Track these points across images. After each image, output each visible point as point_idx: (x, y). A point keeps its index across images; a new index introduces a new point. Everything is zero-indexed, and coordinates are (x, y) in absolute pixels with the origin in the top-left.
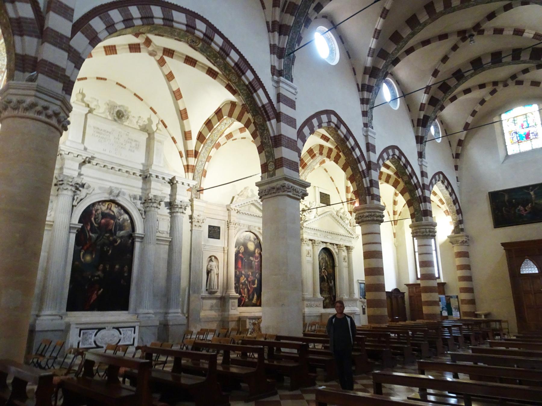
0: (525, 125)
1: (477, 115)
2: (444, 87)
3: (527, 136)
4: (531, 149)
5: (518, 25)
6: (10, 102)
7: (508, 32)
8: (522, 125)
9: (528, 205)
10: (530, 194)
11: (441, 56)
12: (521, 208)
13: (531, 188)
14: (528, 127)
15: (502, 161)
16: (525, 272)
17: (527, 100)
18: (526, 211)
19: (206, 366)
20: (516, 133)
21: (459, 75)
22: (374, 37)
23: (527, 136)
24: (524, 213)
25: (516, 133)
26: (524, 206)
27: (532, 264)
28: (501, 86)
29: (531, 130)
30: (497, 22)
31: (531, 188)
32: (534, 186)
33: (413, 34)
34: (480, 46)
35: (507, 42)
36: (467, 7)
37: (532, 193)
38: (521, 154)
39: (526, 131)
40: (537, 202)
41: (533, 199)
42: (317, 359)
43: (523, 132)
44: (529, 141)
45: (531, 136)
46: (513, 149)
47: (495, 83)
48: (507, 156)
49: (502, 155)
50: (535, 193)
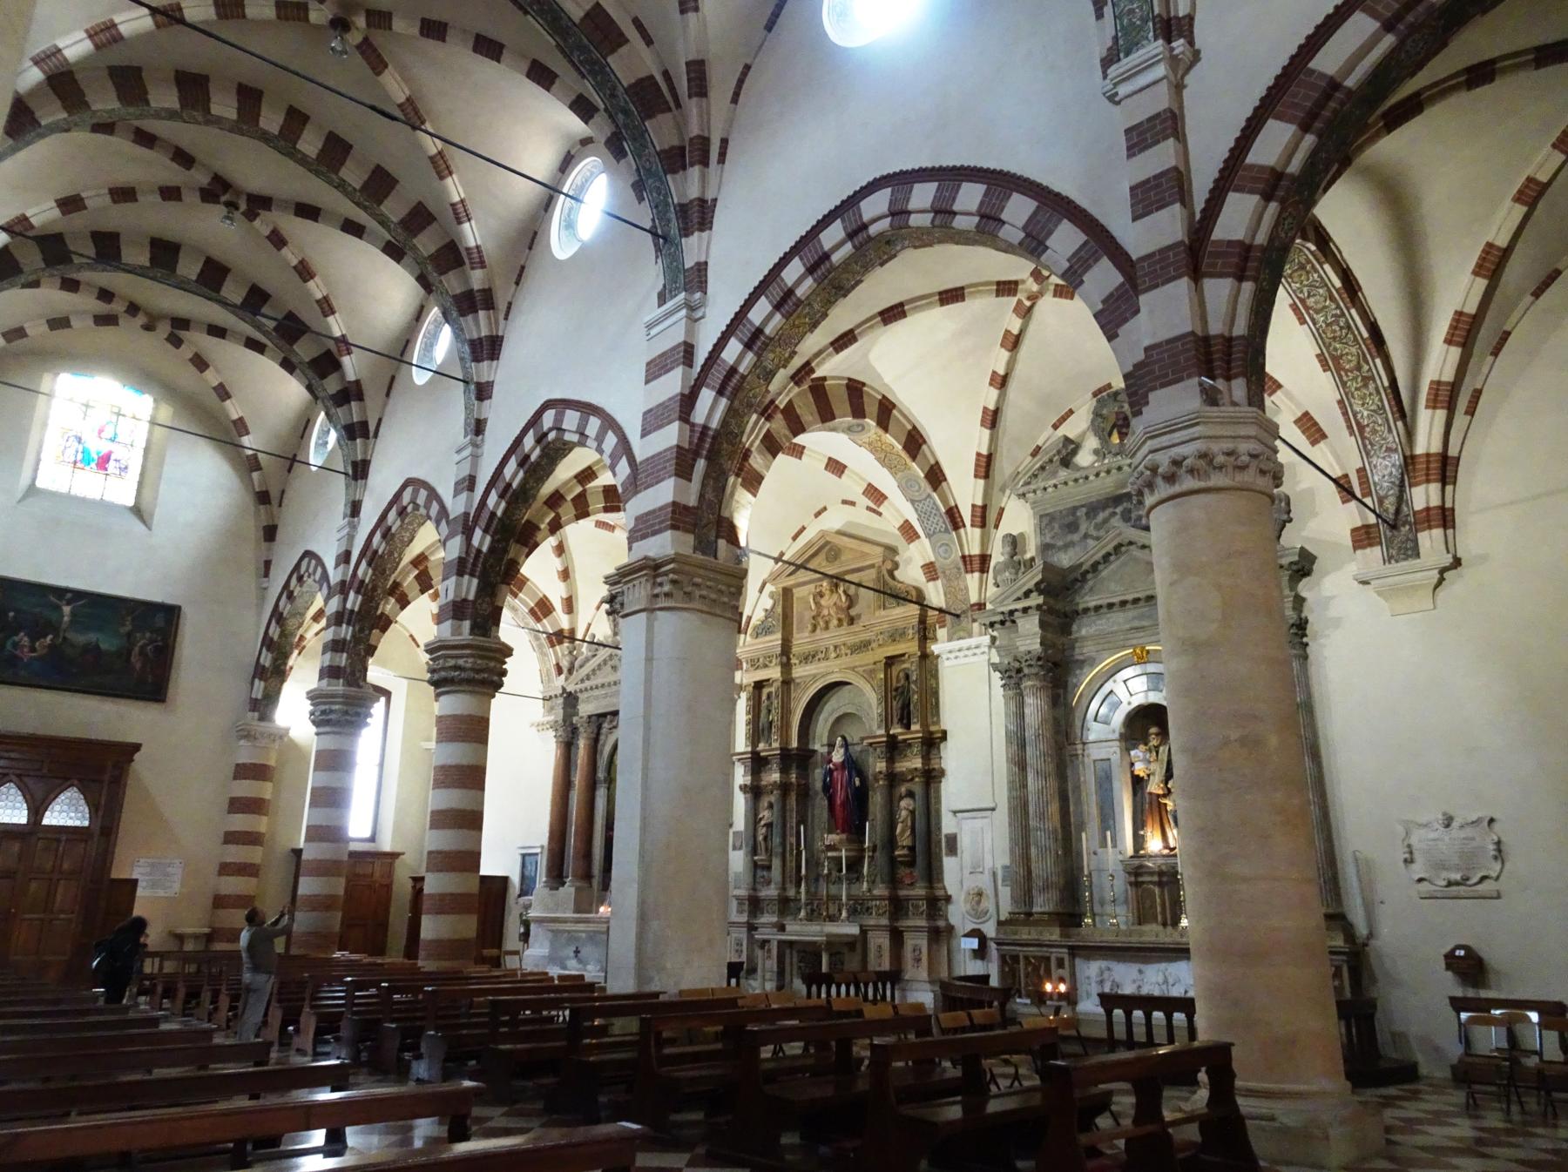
0: (108, 433)
1: (19, 344)
2: (53, 248)
3: (103, 462)
4: (98, 497)
5: (316, 262)
6: (1154, 470)
7: (291, 256)
8: (100, 431)
9: (45, 636)
10: (58, 608)
11: (123, 177)
12: (24, 639)
13: (69, 595)
14: (112, 440)
15: (19, 495)
16: (54, 822)
17: (144, 377)
18: (33, 650)
19: (1176, 1015)
20: (79, 440)
21: (107, 247)
22: (478, 247)
23: (103, 462)
24: (26, 655)
25: (79, 440)
26: (33, 639)
27: (21, 798)
28: (141, 319)
29: (118, 452)
30: (294, 227)
31: (69, 595)
32: (79, 595)
33: (172, 115)
34: (210, 229)
35: (270, 271)
36: (317, 173)
37: (67, 609)
38: (69, 499)
39: (105, 447)
40: (70, 635)
41: (64, 626)
42: (1351, 978)
43: (97, 447)
44: (101, 476)
45: (111, 465)
46: (54, 475)
47: (133, 309)
48: (32, 490)
49: (24, 481)
50: (73, 614)
